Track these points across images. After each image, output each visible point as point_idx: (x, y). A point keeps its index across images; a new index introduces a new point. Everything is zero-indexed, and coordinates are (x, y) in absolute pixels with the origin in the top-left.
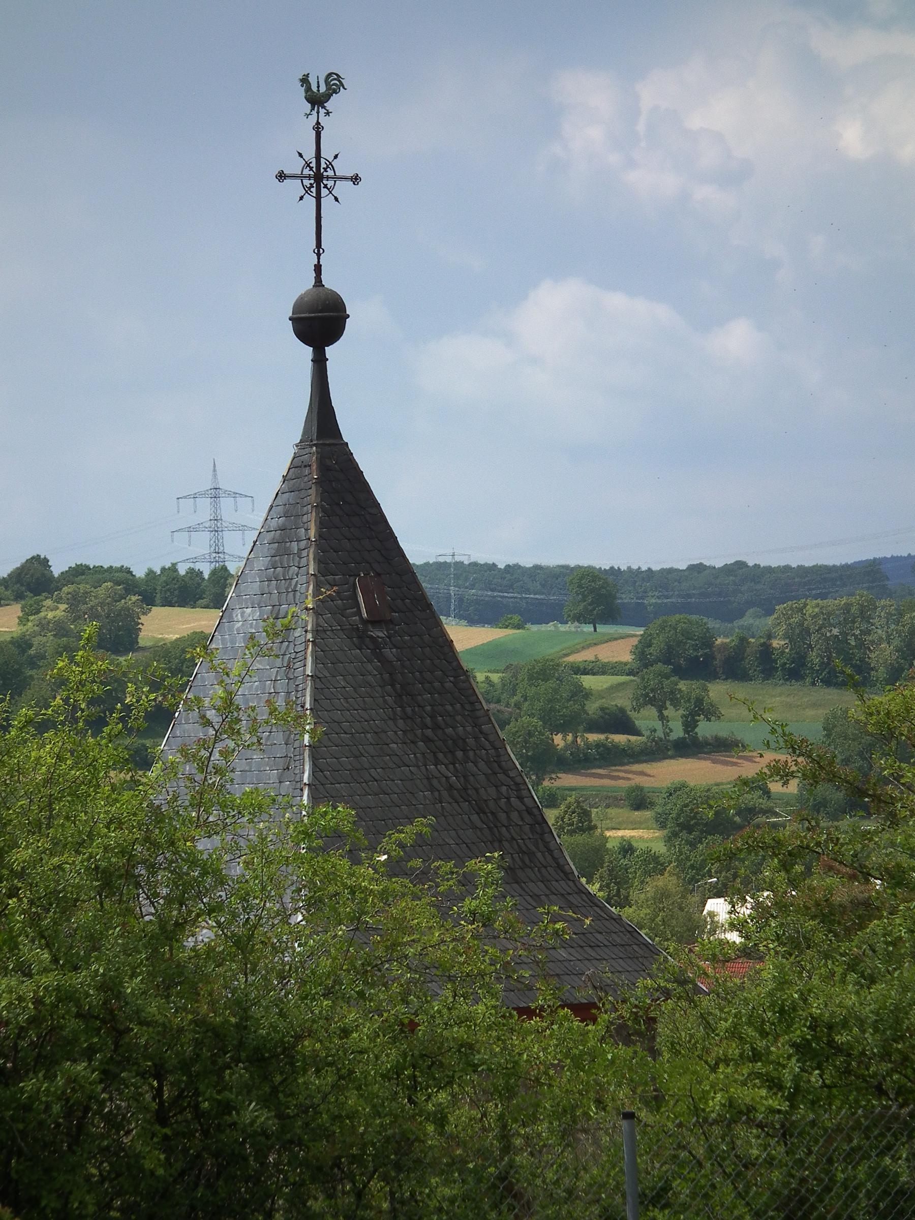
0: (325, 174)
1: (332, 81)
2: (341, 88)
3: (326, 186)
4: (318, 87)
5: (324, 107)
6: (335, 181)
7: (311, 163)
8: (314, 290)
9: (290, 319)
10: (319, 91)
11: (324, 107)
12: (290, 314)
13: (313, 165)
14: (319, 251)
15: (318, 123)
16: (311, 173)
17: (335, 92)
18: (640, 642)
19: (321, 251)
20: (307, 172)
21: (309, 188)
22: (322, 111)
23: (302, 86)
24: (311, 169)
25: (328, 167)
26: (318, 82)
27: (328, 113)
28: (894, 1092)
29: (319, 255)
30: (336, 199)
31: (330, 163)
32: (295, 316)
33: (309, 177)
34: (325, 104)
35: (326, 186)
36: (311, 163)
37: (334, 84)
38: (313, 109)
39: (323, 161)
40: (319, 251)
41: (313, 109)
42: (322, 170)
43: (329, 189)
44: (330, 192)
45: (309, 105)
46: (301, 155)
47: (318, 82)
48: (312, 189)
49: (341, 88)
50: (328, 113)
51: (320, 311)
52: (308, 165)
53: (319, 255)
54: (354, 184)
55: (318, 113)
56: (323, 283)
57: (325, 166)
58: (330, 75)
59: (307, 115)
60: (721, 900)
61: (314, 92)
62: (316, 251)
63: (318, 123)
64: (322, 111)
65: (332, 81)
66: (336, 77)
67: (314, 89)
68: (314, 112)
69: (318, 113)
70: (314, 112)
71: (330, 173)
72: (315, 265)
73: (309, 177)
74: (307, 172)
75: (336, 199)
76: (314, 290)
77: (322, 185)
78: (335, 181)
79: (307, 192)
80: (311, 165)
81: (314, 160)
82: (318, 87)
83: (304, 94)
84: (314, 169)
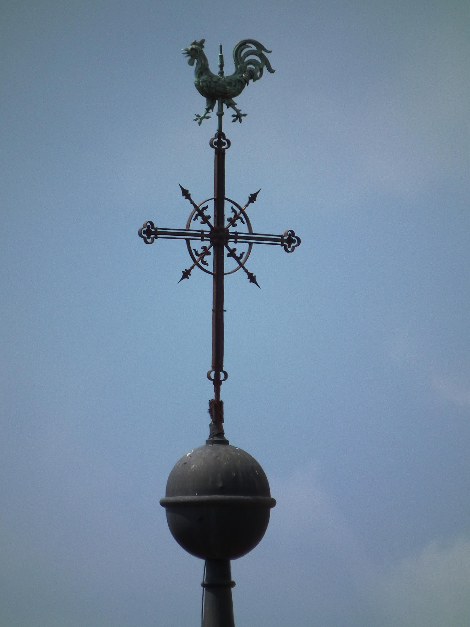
0: (232, 229)
1: (247, 54)
2: (265, 69)
3: (232, 253)
4: (221, 66)
5: (231, 105)
6: (251, 244)
7: (205, 208)
8: (209, 450)
9: (163, 504)
10: (222, 73)
11: (231, 105)
12: (162, 495)
13: (210, 212)
14: (217, 375)
15: (220, 134)
16: (206, 228)
17: (253, 76)
18: (219, 79)
19: (222, 376)
20: (197, 225)
21: (202, 256)
22: (228, 112)
23: (191, 63)
24: (205, 220)
25: (237, 217)
26: (221, 57)
27: (238, 117)
28: (198, 50)
29: (217, 383)
30: (252, 278)
31: (242, 211)
32: (172, 499)
33: (201, 235)
34: (235, 99)
35: (232, 253)
36: (205, 208)
37: (250, 62)
38: (210, 108)
39: (228, 206)
40: (217, 375)
41: (210, 108)
42: (226, 223)
43: (238, 259)
44: (241, 265)
45: (204, 100)
46: (186, 194)
47: (221, 57)
48: (206, 258)
49: (265, 69)
50: (238, 117)
51: (221, 491)
52: (201, 213)
53: (217, 383)
54: (287, 251)
55: (220, 115)
56: (227, 436)
57: (232, 215)
58: (243, 44)
59: (200, 119)
60: (240, 211)
61: (212, 76)
62: (212, 375)
63: (220, 134)
64: (228, 112)
65: (247, 54)
66: (254, 48)
67: (214, 69)
68: (213, 114)
69: (220, 115)
70: (213, 114)
71: (241, 228)
72: (211, 403)
73: (201, 235)
74: (197, 225)
75: (252, 278)
76: (209, 450)
77: (226, 252)
78: (251, 244)
79: (196, 263)
80: (206, 213)
81: (211, 204)
82: (221, 66)
83: (193, 79)
84: (211, 221)
